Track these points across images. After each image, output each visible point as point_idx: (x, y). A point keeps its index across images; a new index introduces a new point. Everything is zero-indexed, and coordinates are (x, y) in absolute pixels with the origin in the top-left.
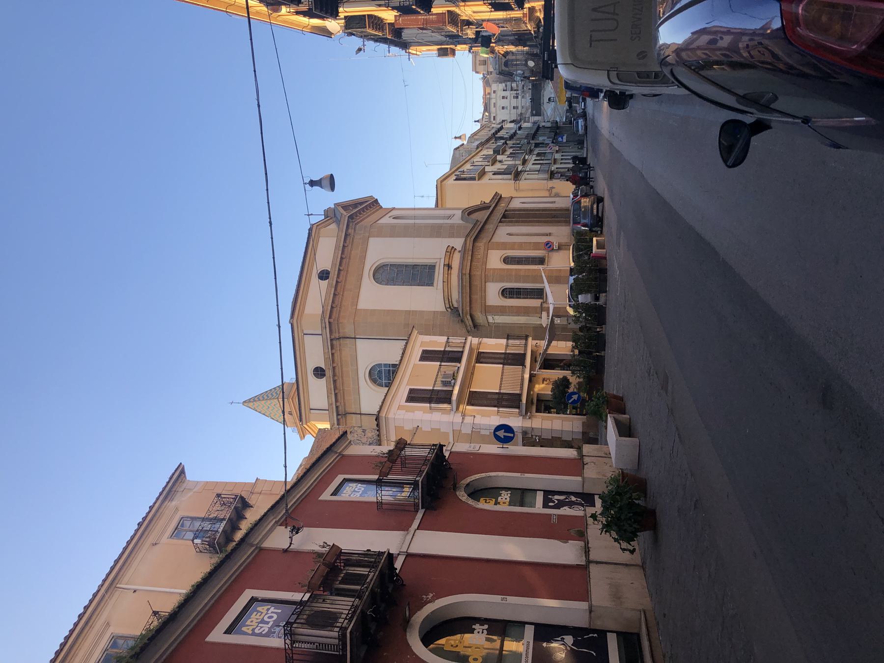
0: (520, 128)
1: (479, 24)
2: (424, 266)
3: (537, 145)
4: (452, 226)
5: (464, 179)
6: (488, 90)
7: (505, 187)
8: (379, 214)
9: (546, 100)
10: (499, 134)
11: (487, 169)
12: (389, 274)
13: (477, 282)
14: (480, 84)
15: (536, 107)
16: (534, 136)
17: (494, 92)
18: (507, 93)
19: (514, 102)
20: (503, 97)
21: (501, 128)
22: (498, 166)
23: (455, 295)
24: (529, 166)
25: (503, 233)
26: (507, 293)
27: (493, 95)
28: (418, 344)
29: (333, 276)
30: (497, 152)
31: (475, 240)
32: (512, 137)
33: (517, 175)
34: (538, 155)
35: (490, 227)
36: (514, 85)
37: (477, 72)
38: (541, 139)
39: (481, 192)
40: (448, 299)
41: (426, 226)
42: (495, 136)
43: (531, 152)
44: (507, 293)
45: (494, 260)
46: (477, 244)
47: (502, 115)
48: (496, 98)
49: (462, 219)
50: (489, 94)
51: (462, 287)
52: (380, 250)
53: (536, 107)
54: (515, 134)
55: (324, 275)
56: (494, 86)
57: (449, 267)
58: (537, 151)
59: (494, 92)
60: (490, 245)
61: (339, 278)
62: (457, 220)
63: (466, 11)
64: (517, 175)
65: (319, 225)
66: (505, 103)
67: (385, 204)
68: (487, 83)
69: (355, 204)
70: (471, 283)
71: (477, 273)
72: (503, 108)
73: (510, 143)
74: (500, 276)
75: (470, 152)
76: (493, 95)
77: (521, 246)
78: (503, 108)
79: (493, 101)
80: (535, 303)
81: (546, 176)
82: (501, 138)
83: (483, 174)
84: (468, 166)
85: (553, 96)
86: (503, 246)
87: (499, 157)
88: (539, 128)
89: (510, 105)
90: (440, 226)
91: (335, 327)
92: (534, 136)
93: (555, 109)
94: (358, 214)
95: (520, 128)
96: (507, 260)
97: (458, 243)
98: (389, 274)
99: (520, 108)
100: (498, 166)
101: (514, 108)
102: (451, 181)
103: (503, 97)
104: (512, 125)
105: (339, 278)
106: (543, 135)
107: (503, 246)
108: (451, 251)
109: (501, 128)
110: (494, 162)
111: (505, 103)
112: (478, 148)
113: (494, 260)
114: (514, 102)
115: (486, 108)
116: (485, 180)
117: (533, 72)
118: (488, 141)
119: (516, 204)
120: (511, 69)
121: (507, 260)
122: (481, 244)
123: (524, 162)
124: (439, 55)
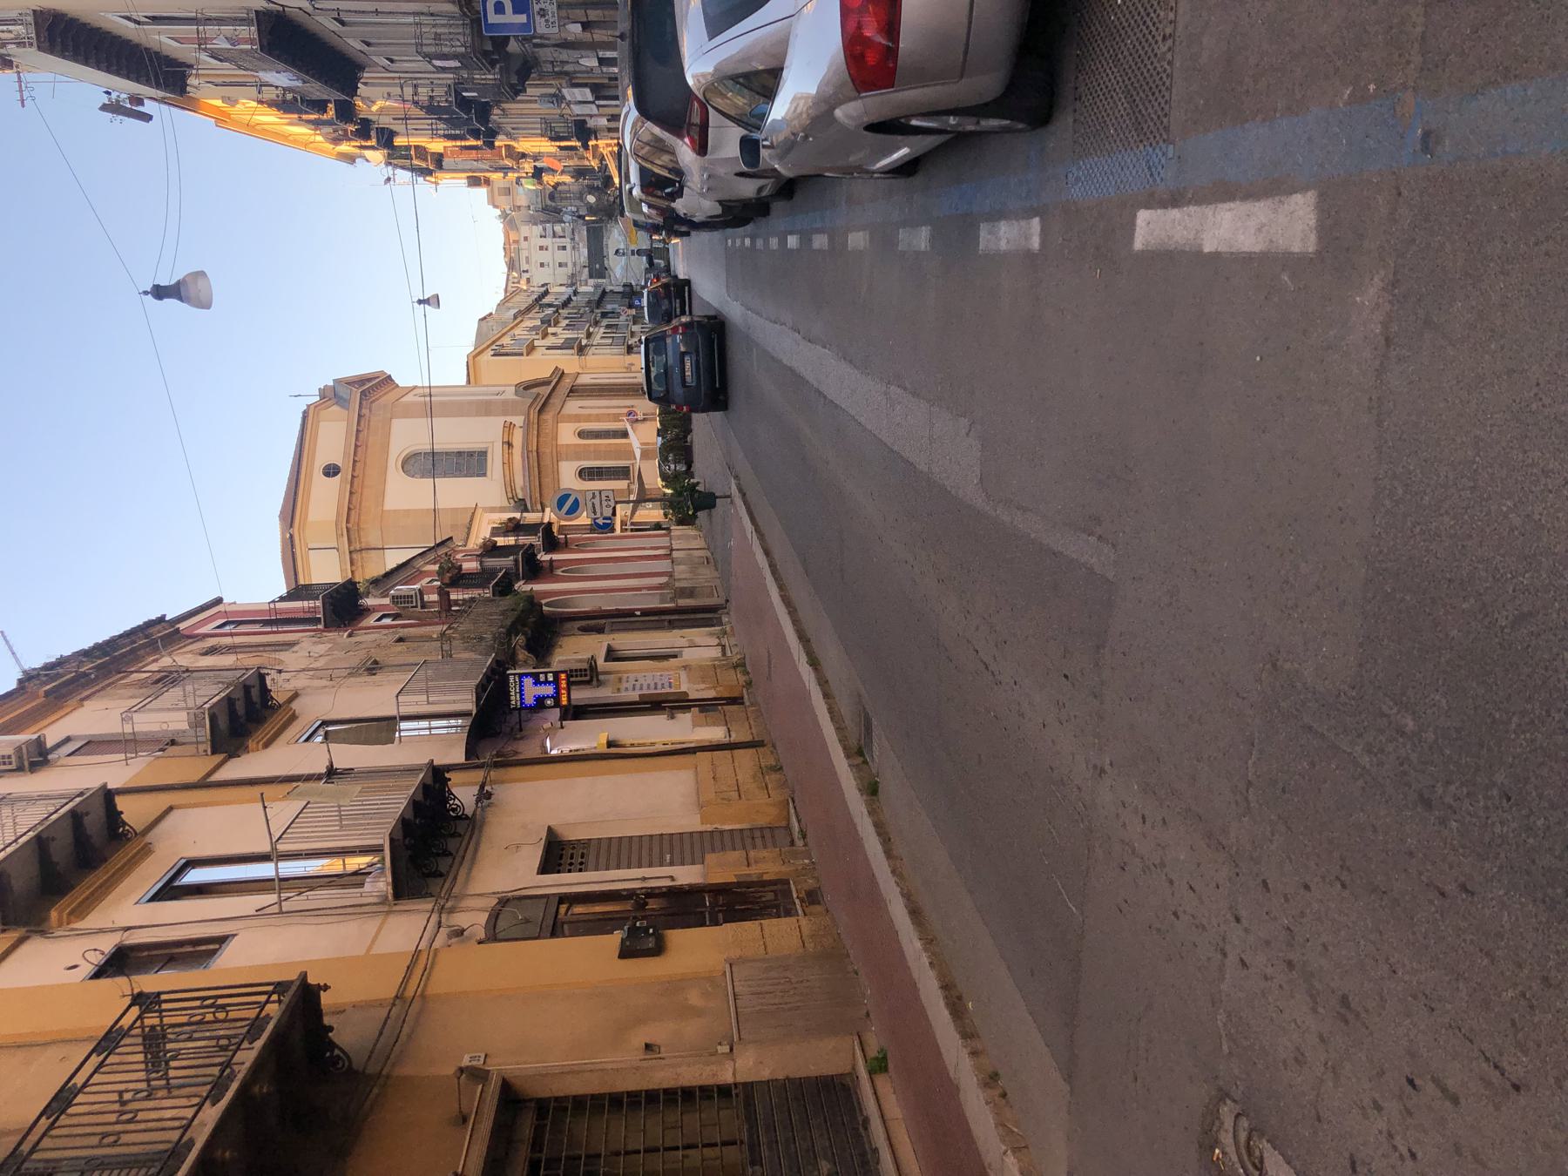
0: (575, 293)
1: (536, 158)
2: (471, 454)
3: (604, 315)
4: (505, 402)
5: (507, 355)
6: (513, 236)
7: (568, 362)
8: (391, 396)
9: (611, 252)
10: (546, 300)
11: (536, 343)
12: (432, 464)
13: (546, 461)
14: (498, 227)
15: (597, 266)
16: (599, 303)
17: (526, 239)
18: (548, 242)
19: (562, 256)
20: (541, 248)
21: (546, 293)
22: (550, 341)
23: (519, 481)
24: (597, 339)
25: (574, 406)
26: (587, 474)
27: (524, 244)
28: (485, 523)
29: (346, 472)
30: (546, 322)
31: (540, 412)
32: (566, 304)
33: (581, 350)
34: (608, 326)
35: (556, 401)
36: (558, 228)
37: (496, 207)
38: (609, 307)
39: (541, 365)
40: (509, 485)
41: (470, 403)
42: (539, 302)
43: (596, 323)
44: (587, 474)
45: (567, 434)
46: (544, 417)
47: (540, 277)
48: (529, 249)
49: (516, 393)
50: (516, 242)
51: (528, 469)
52: (407, 436)
53: (597, 266)
54: (569, 300)
55: (331, 471)
56: (525, 230)
57: (510, 445)
58: (605, 322)
59: (526, 239)
60: (559, 418)
61: (355, 473)
62: (510, 393)
63: (523, 145)
64: (581, 350)
65: (316, 406)
66: (545, 257)
67: (402, 380)
68: (509, 222)
69: (361, 381)
70: (539, 463)
71: (546, 450)
72: (542, 265)
73: (564, 312)
74: (577, 453)
75: (505, 324)
76: (524, 244)
77: (598, 418)
78: (542, 265)
79: (524, 254)
80: (621, 484)
81: (623, 349)
82: (550, 305)
83: (531, 348)
84: (506, 340)
85: (622, 246)
86: (577, 418)
87: (551, 330)
88: (604, 293)
89: (556, 261)
90: (488, 403)
91: (354, 535)
92: (599, 303)
93: (626, 268)
94: (368, 393)
95: (575, 293)
96: (582, 434)
97: (519, 420)
98: (432, 464)
99: (570, 265)
100: (550, 341)
101: (560, 265)
102: (487, 356)
103: (541, 248)
104: (563, 289)
105: (355, 473)
106: (613, 302)
107: (577, 418)
108: (509, 427)
109: (546, 293)
110: (545, 335)
111: (545, 257)
112: (515, 317)
113: (567, 434)
114: (562, 256)
115: (511, 265)
116: (537, 355)
117: (591, 210)
118: (529, 309)
119: (585, 379)
120: (559, 204)
121: (582, 434)
122: (548, 416)
123: (589, 335)
124: (470, 185)
